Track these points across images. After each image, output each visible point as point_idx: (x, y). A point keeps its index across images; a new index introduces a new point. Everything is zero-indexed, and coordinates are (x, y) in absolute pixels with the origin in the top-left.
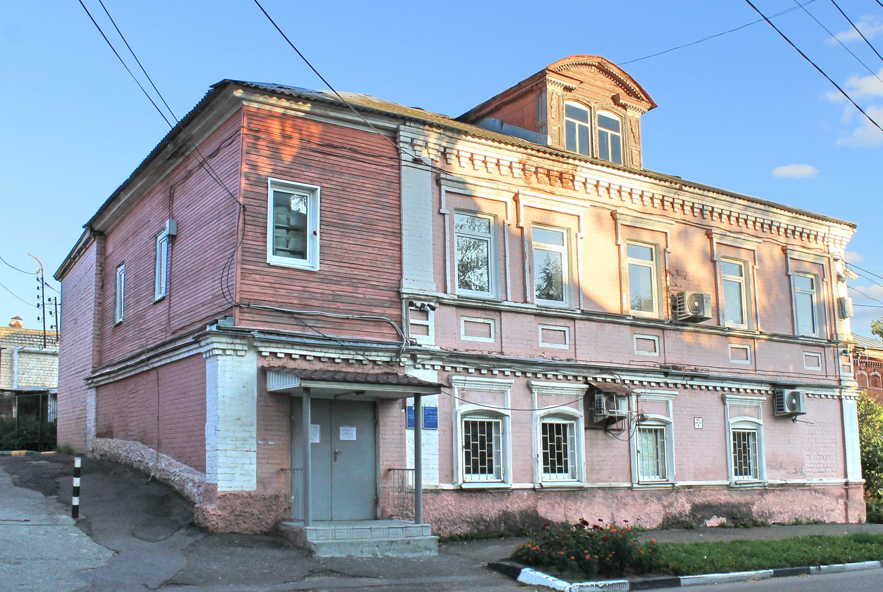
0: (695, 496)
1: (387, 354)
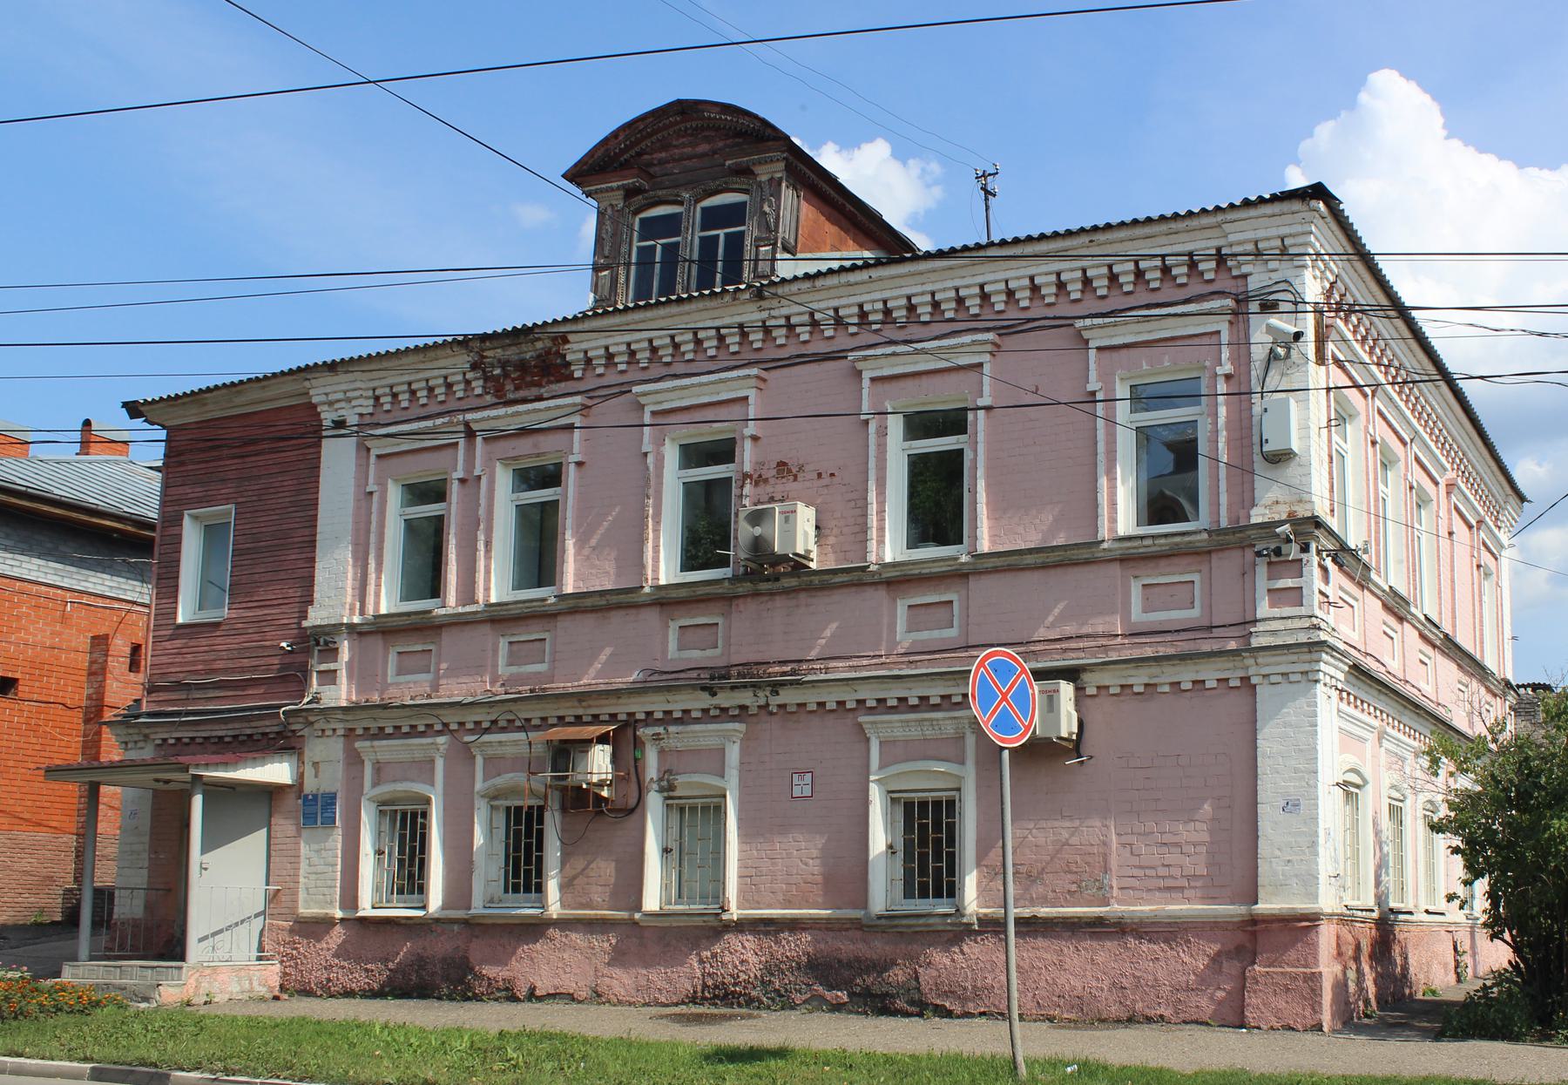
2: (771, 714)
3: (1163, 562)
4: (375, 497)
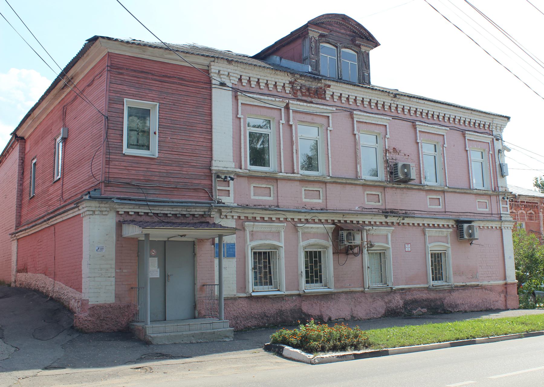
0: (406, 295)
3: (482, 196)
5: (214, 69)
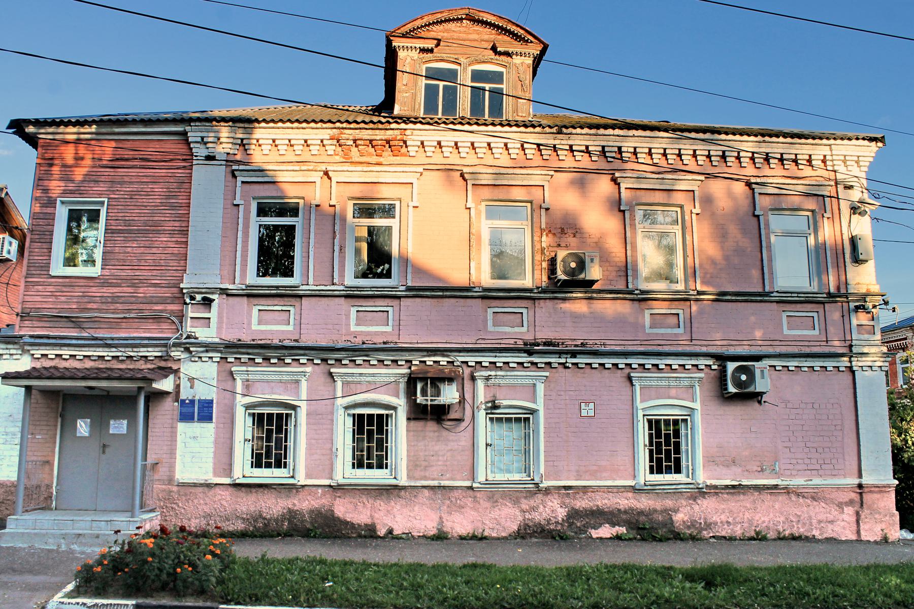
0: (575, 498)
1: (159, 349)
2: (568, 368)
4: (241, 208)
5: (193, 136)
